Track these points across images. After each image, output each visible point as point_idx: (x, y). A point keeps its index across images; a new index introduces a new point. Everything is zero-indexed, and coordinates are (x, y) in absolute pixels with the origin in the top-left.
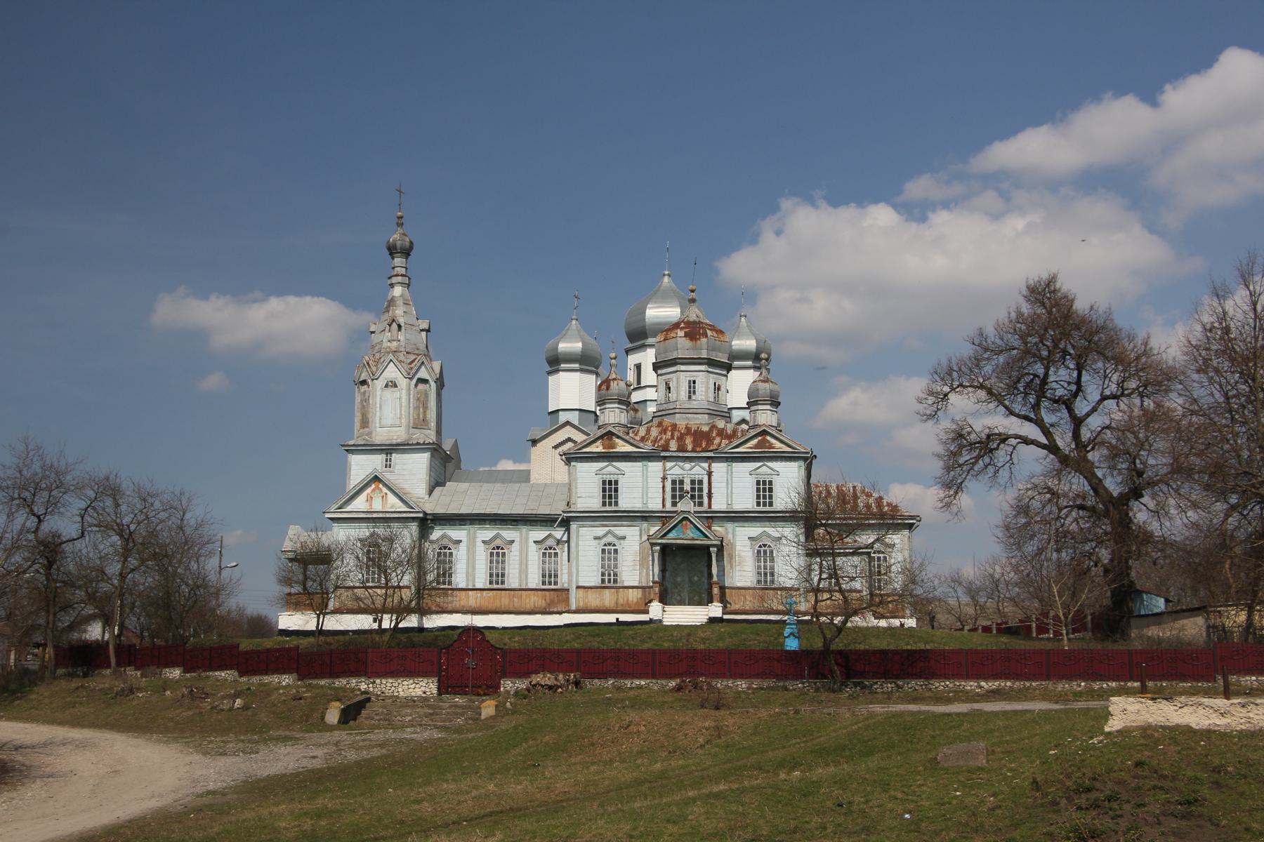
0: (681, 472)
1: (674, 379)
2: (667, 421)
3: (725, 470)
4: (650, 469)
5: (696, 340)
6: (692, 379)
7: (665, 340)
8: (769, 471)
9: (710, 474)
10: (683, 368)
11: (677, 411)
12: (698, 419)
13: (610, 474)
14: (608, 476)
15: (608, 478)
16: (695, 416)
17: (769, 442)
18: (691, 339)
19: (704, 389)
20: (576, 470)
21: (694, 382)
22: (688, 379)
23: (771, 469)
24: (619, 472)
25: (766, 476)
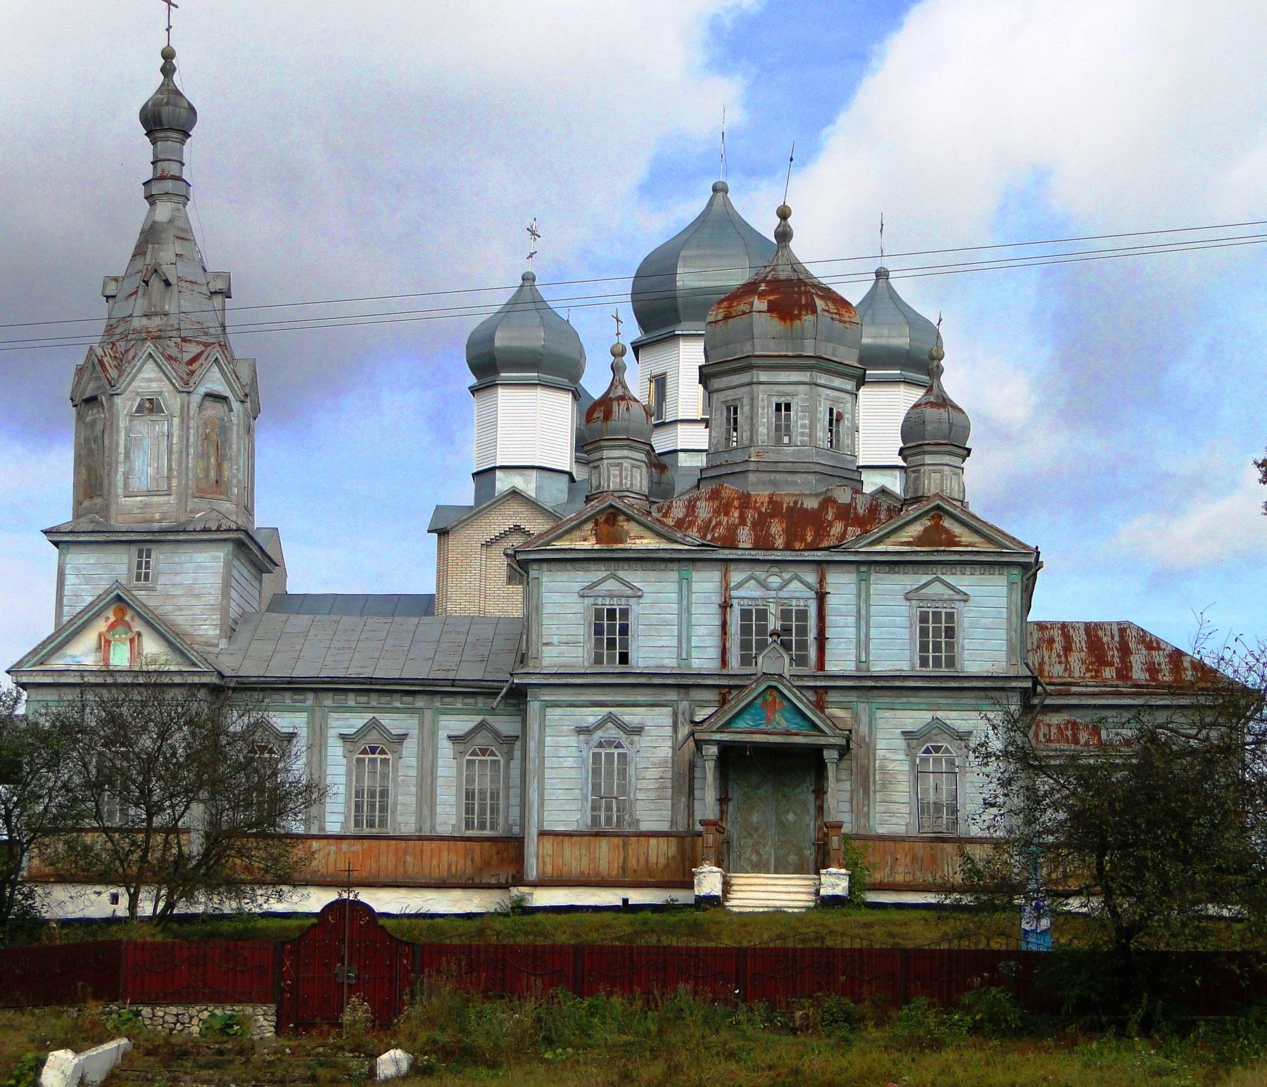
0: (759, 593)
1: (746, 401)
2: (730, 488)
4: (695, 587)
5: (792, 318)
6: (782, 400)
7: (726, 318)
8: (948, 593)
9: (821, 597)
10: (764, 376)
11: (752, 467)
12: (796, 483)
13: (611, 597)
14: (607, 601)
21: (788, 407)
22: (775, 400)
24: (630, 592)
25: (940, 604)
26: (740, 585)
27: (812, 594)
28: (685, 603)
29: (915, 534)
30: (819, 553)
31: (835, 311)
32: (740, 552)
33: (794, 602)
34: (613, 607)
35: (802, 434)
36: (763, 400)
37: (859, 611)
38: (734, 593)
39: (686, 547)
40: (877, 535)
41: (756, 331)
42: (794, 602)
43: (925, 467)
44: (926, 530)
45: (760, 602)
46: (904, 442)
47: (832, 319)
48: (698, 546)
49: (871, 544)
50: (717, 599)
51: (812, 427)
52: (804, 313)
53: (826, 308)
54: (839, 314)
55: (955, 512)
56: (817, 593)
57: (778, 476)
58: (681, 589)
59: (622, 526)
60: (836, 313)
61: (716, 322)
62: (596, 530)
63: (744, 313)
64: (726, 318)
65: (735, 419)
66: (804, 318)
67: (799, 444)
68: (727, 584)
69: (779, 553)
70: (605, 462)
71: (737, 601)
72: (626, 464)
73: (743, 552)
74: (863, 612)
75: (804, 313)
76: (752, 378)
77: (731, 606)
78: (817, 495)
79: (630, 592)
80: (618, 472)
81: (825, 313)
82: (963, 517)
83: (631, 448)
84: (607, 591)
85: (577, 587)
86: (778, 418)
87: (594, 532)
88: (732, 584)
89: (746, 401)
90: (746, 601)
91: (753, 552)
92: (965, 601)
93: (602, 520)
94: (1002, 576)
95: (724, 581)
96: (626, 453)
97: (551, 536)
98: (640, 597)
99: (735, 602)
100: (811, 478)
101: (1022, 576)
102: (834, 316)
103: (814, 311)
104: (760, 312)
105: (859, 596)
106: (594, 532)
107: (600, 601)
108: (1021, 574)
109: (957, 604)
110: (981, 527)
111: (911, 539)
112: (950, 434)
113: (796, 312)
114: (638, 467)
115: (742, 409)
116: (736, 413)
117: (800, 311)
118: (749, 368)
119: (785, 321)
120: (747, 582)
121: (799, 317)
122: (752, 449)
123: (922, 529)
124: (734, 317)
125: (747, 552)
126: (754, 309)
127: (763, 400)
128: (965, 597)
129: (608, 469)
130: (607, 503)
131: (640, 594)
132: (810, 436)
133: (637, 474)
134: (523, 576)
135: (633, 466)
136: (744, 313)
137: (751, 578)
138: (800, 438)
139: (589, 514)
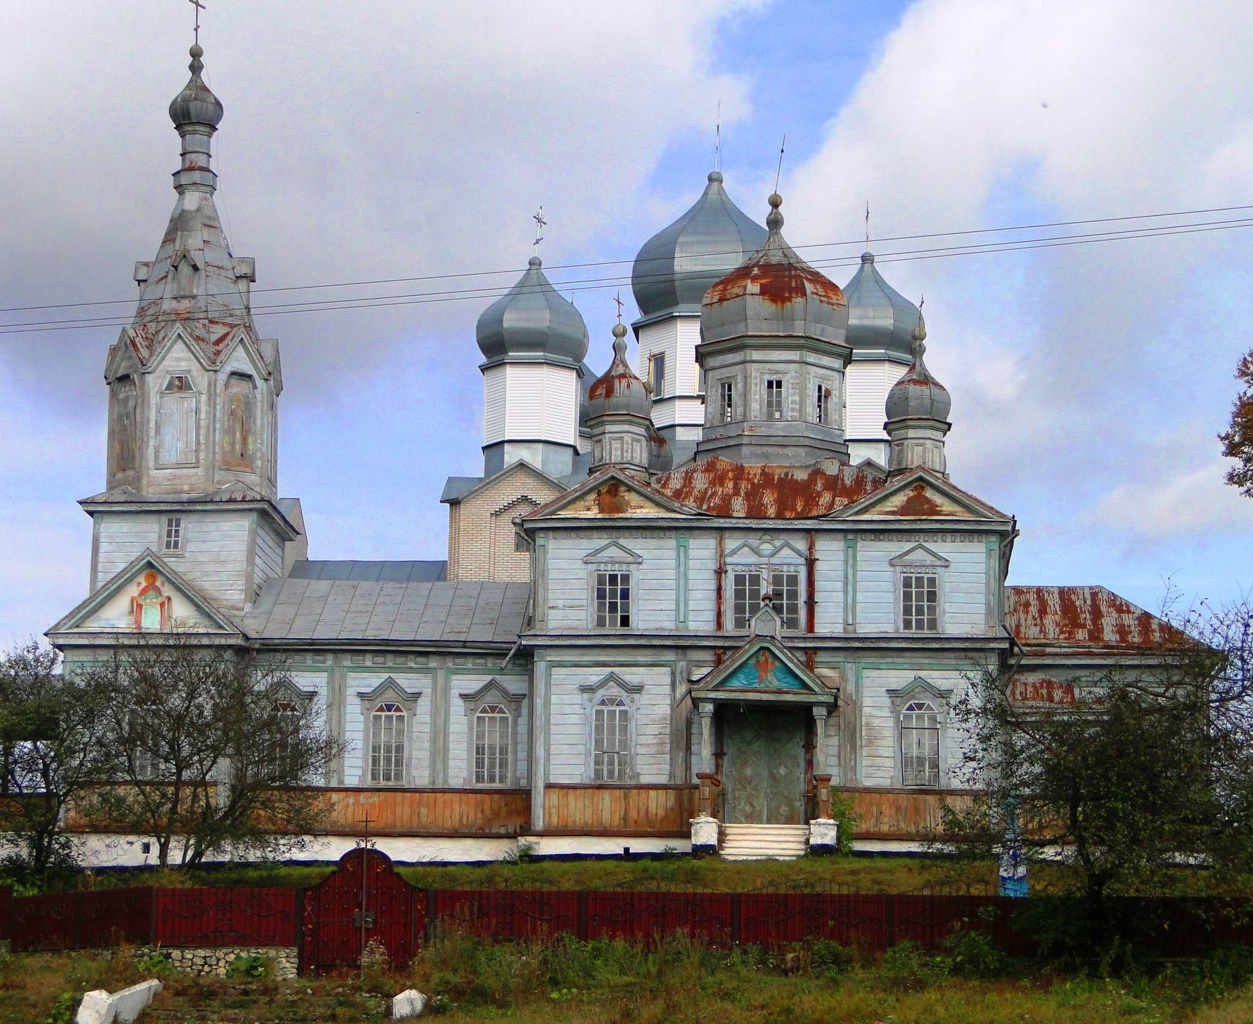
0: (753, 559)
1: (739, 378)
2: (725, 461)
3: (841, 555)
4: (692, 553)
6: (774, 378)
7: (721, 300)
8: (929, 559)
9: (811, 563)
10: (756, 355)
11: (746, 440)
12: (786, 456)
13: (613, 563)
14: (609, 567)
15: (609, 569)
16: (780, 451)
17: (929, 501)
18: (774, 300)
19: (797, 398)
20: (545, 553)
21: (779, 384)
22: (767, 377)
23: (934, 554)
24: (630, 559)
25: (923, 570)
26: (734, 552)
27: (802, 561)
28: (682, 568)
29: (899, 504)
30: (809, 522)
31: (823, 294)
32: (734, 521)
33: (785, 568)
34: (615, 573)
35: (793, 410)
36: (756, 378)
37: (846, 576)
38: (728, 560)
39: (684, 516)
40: (864, 505)
41: (749, 313)
42: (785, 568)
43: (909, 441)
44: (910, 500)
45: (753, 568)
46: (889, 417)
47: (821, 301)
48: (695, 515)
49: (857, 513)
50: (714, 565)
51: (802, 403)
52: (794, 295)
53: (815, 291)
54: (828, 297)
55: (936, 483)
56: (806, 559)
57: (770, 450)
58: (678, 556)
59: (623, 497)
60: (824, 296)
61: (711, 304)
62: (599, 500)
63: (738, 296)
64: (721, 300)
65: (730, 396)
66: (794, 300)
67: (790, 419)
68: (722, 551)
69: (771, 522)
70: (607, 436)
71: (732, 566)
72: (627, 438)
73: (737, 521)
74: (850, 578)
75: (794, 295)
76: (745, 355)
77: (726, 571)
78: (806, 467)
79: (630, 559)
80: (619, 446)
81: (815, 296)
82: (944, 488)
83: (631, 423)
84: (609, 557)
85: (583, 553)
86: (770, 395)
87: (596, 502)
88: (727, 551)
89: (739, 378)
90: (740, 567)
91: (747, 521)
92: (946, 567)
93: (604, 491)
94: (981, 544)
95: (719, 549)
96: (626, 427)
97: (556, 506)
98: (640, 563)
99: (729, 568)
100: (802, 451)
101: (1000, 544)
102: (822, 298)
103: (804, 294)
104: (753, 294)
105: (846, 562)
106: (596, 502)
107: (602, 567)
108: (998, 541)
109: (939, 570)
110: (961, 497)
111: (896, 509)
112: (932, 409)
113: (787, 295)
114: (638, 441)
115: (736, 386)
116: (730, 390)
117: (790, 293)
118: (743, 347)
119: (777, 304)
120: (740, 549)
121: (790, 299)
122: (745, 424)
123: (905, 499)
124: (729, 299)
125: (741, 521)
126: (748, 292)
127: (756, 378)
128: (946, 563)
129: (610, 444)
130: (609, 475)
131: (640, 560)
132: (800, 411)
133: (637, 447)
134: (530, 544)
135: (633, 440)
136: (738, 296)
137: (745, 545)
138: (790, 414)
139: (592, 485)
